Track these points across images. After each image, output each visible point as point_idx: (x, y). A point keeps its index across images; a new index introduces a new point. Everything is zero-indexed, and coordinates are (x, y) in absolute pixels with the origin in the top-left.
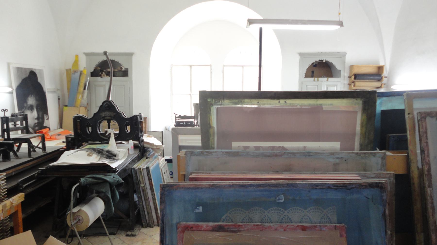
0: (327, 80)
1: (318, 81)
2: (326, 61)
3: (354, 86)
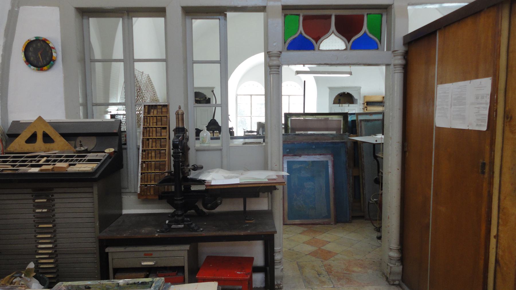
0: (349, 106)
1: (342, 106)
3: (366, 110)
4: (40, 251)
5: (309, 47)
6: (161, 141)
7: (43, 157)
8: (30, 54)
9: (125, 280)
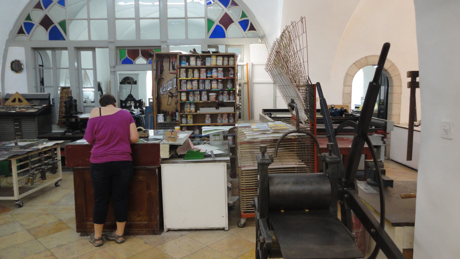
5: (131, 63)
7: (17, 107)
8: (13, 66)
9: (14, 111)
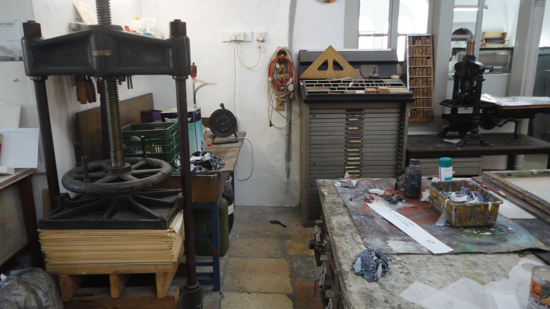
2: (465, 29)
4: (349, 163)
6: (427, 69)
9: (362, 92)
